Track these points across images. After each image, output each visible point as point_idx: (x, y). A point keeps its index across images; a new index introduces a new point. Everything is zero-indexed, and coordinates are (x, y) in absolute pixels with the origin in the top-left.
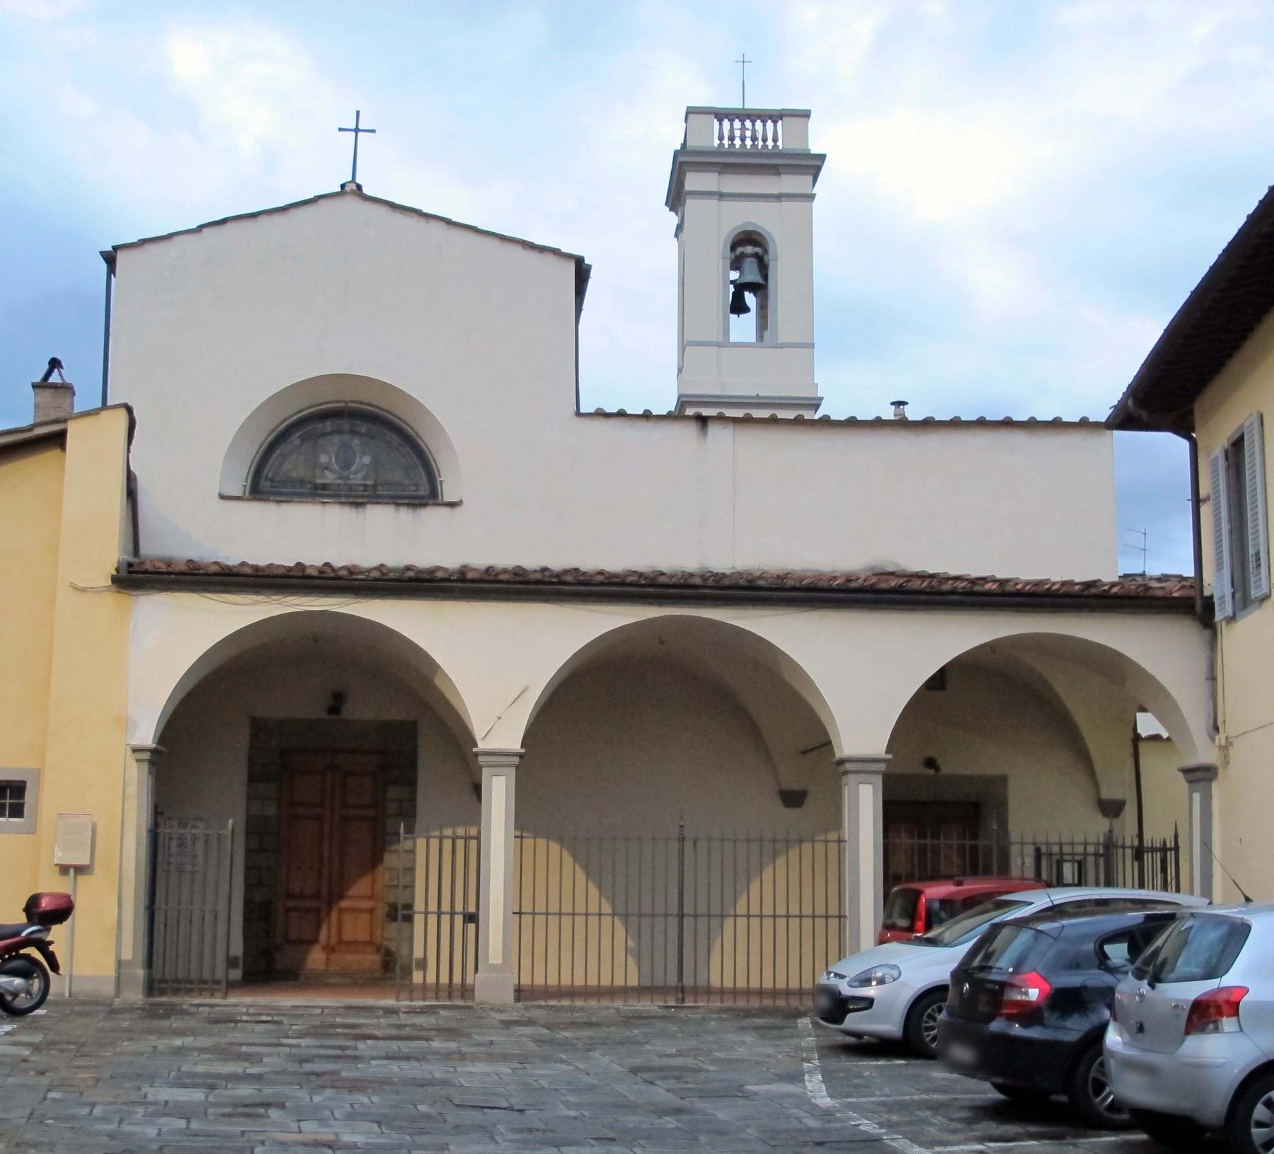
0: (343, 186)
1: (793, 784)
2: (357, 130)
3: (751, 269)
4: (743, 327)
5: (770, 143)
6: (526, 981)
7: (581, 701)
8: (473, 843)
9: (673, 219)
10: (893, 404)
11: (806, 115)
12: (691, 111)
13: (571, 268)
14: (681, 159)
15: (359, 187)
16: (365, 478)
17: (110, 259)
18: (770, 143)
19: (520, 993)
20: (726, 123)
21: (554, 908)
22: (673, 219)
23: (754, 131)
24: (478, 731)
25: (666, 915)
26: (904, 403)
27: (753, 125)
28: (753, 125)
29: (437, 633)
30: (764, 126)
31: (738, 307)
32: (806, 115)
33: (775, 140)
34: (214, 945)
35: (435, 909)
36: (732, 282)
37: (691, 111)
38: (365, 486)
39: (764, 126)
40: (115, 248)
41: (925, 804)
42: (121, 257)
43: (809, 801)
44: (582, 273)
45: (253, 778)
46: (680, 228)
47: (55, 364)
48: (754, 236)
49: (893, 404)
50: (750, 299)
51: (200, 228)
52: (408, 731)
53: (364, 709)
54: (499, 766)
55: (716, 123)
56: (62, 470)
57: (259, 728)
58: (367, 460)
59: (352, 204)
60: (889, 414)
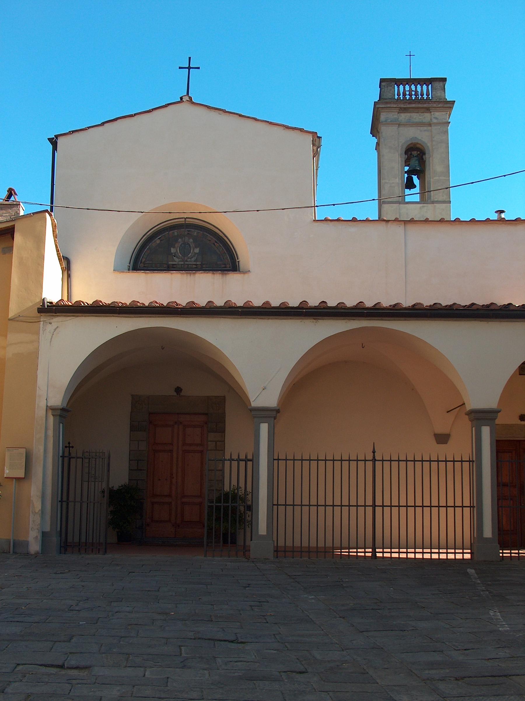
0: (181, 98)
1: (440, 429)
2: (189, 68)
3: (417, 162)
4: (413, 195)
5: (425, 97)
6: (281, 543)
7: (308, 379)
8: (250, 464)
9: (375, 140)
10: (496, 212)
11: (444, 80)
12: (382, 81)
13: (310, 138)
14: (377, 106)
15: (190, 98)
16: (196, 261)
17: (54, 142)
18: (425, 97)
19: (277, 550)
20: (401, 87)
21: (395, 503)
22: (375, 140)
23: (416, 91)
24: (251, 400)
25: (365, 506)
26: (502, 212)
27: (416, 88)
28: (416, 88)
29: (219, 336)
30: (422, 87)
31: (410, 185)
32: (444, 80)
33: (428, 95)
34: (97, 522)
35: (70, 504)
36: (406, 172)
37: (382, 81)
38: (196, 265)
39: (422, 87)
40: (57, 136)
41: (520, 441)
42: (61, 142)
43: (451, 442)
44: (316, 140)
45: (133, 428)
46: (378, 144)
47: (11, 193)
48: (418, 146)
49: (496, 212)
50: (416, 180)
51: (103, 124)
52: (221, 401)
53: (197, 389)
54: (264, 417)
55: (396, 87)
56: (10, 249)
57: (137, 401)
58: (197, 250)
59: (185, 107)
60: (495, 217)
